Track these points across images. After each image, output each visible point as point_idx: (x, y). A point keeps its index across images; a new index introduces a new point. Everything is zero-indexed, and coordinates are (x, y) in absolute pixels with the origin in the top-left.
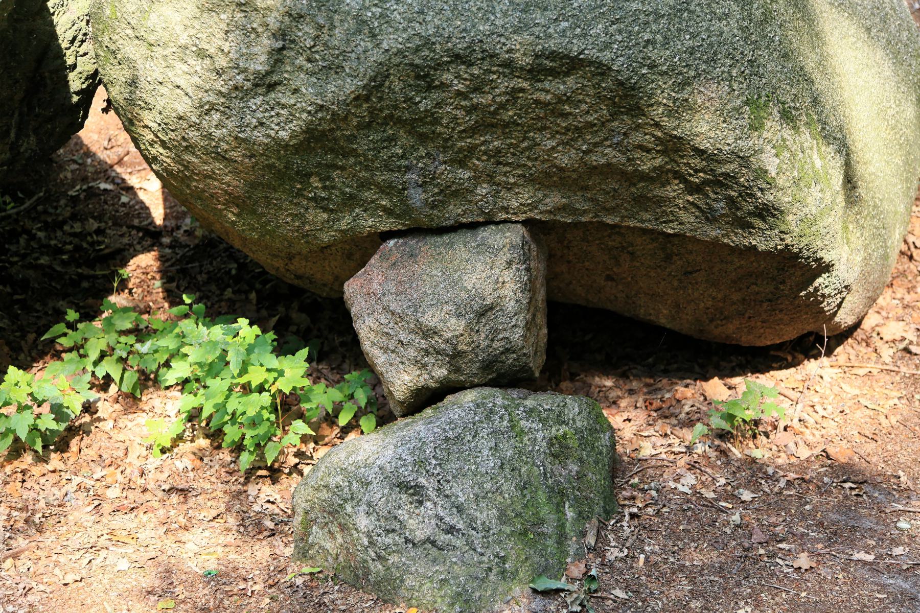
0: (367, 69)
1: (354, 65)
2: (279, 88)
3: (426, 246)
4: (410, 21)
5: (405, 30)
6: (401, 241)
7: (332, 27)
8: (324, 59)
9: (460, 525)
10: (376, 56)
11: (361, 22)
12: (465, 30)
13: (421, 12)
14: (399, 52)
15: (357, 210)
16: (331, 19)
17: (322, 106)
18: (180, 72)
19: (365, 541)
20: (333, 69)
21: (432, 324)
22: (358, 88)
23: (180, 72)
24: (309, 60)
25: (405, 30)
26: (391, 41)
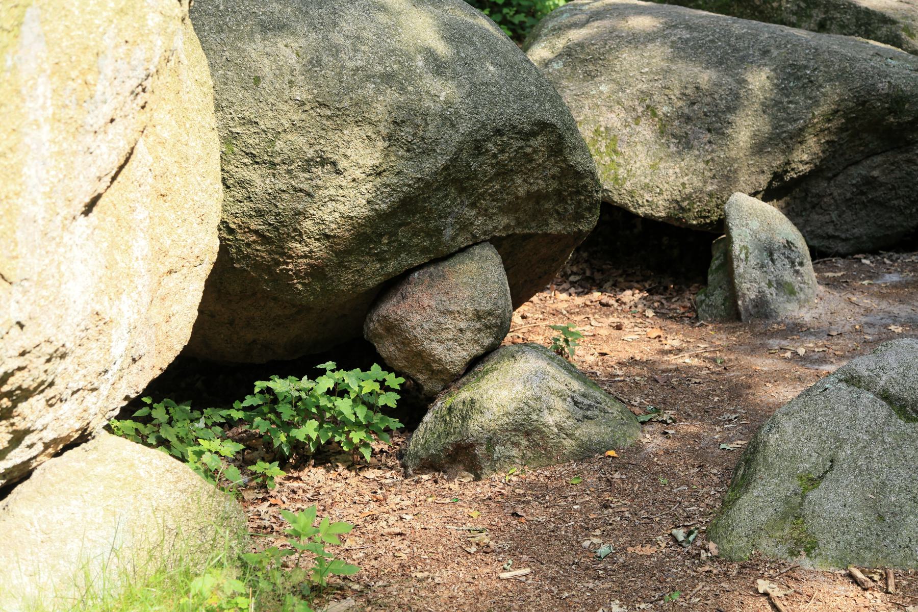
0: (452, 149)
1: (444, 147)
2: (385, 174)
3: (446, 267)
4: (471, 113)
5: (470, 119)
6: (421, 272)
7: (427, 124)
8: (419, 148)
9: (593, 403)
10: (457, 138)
11: (445, 119)
12: (501, 114)
13: (475, 107)
14: (470, 133)
15: (402, 255)
16: (425, 120)
17: (419, 179)
18: (303, 179)
19: (556, 430)
20: (428, 152)
21: (488, 308)
22: (447, 161)
23: (303, 179)
24: (408, 151)
25: (470, 119)
26: (464, 128)
